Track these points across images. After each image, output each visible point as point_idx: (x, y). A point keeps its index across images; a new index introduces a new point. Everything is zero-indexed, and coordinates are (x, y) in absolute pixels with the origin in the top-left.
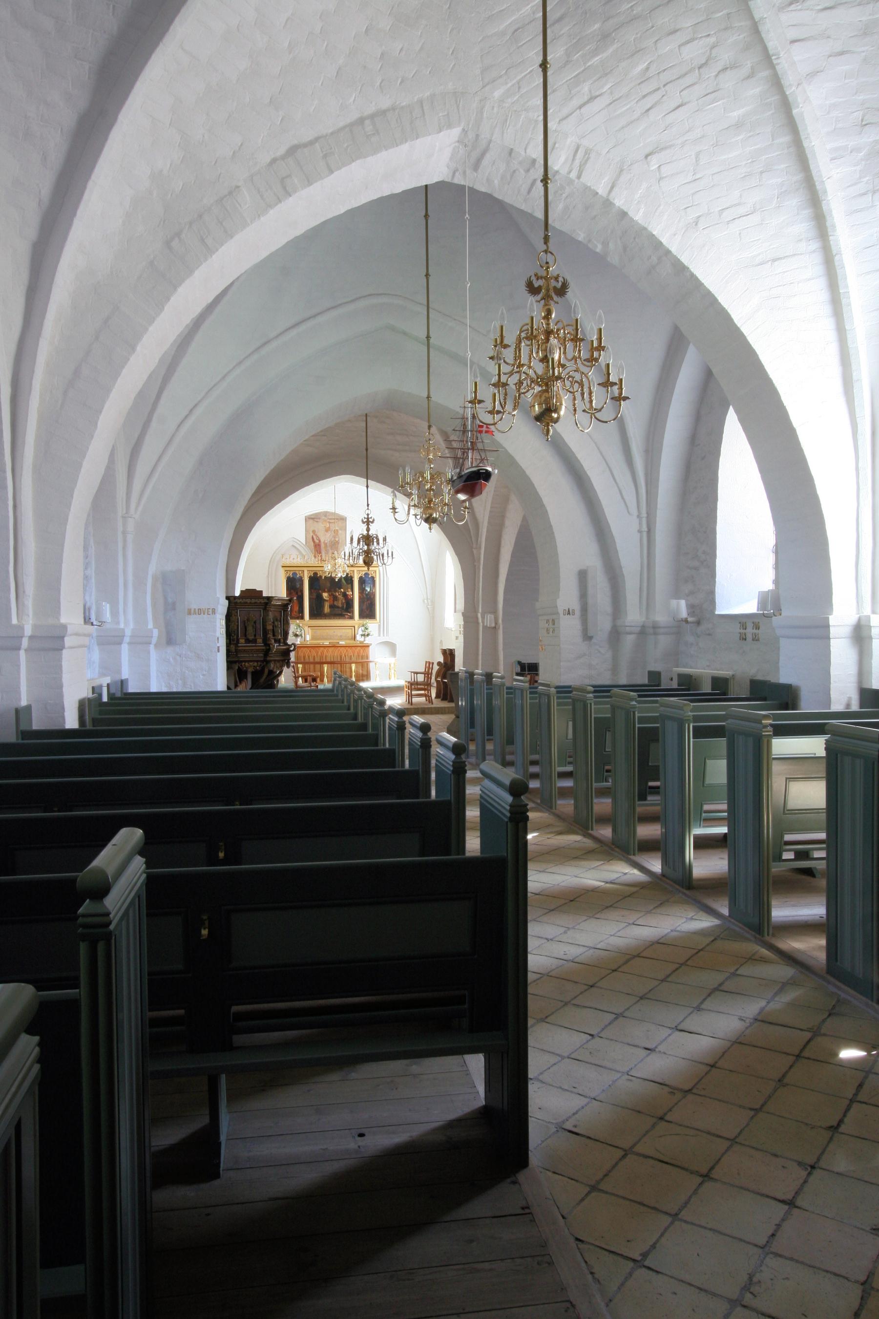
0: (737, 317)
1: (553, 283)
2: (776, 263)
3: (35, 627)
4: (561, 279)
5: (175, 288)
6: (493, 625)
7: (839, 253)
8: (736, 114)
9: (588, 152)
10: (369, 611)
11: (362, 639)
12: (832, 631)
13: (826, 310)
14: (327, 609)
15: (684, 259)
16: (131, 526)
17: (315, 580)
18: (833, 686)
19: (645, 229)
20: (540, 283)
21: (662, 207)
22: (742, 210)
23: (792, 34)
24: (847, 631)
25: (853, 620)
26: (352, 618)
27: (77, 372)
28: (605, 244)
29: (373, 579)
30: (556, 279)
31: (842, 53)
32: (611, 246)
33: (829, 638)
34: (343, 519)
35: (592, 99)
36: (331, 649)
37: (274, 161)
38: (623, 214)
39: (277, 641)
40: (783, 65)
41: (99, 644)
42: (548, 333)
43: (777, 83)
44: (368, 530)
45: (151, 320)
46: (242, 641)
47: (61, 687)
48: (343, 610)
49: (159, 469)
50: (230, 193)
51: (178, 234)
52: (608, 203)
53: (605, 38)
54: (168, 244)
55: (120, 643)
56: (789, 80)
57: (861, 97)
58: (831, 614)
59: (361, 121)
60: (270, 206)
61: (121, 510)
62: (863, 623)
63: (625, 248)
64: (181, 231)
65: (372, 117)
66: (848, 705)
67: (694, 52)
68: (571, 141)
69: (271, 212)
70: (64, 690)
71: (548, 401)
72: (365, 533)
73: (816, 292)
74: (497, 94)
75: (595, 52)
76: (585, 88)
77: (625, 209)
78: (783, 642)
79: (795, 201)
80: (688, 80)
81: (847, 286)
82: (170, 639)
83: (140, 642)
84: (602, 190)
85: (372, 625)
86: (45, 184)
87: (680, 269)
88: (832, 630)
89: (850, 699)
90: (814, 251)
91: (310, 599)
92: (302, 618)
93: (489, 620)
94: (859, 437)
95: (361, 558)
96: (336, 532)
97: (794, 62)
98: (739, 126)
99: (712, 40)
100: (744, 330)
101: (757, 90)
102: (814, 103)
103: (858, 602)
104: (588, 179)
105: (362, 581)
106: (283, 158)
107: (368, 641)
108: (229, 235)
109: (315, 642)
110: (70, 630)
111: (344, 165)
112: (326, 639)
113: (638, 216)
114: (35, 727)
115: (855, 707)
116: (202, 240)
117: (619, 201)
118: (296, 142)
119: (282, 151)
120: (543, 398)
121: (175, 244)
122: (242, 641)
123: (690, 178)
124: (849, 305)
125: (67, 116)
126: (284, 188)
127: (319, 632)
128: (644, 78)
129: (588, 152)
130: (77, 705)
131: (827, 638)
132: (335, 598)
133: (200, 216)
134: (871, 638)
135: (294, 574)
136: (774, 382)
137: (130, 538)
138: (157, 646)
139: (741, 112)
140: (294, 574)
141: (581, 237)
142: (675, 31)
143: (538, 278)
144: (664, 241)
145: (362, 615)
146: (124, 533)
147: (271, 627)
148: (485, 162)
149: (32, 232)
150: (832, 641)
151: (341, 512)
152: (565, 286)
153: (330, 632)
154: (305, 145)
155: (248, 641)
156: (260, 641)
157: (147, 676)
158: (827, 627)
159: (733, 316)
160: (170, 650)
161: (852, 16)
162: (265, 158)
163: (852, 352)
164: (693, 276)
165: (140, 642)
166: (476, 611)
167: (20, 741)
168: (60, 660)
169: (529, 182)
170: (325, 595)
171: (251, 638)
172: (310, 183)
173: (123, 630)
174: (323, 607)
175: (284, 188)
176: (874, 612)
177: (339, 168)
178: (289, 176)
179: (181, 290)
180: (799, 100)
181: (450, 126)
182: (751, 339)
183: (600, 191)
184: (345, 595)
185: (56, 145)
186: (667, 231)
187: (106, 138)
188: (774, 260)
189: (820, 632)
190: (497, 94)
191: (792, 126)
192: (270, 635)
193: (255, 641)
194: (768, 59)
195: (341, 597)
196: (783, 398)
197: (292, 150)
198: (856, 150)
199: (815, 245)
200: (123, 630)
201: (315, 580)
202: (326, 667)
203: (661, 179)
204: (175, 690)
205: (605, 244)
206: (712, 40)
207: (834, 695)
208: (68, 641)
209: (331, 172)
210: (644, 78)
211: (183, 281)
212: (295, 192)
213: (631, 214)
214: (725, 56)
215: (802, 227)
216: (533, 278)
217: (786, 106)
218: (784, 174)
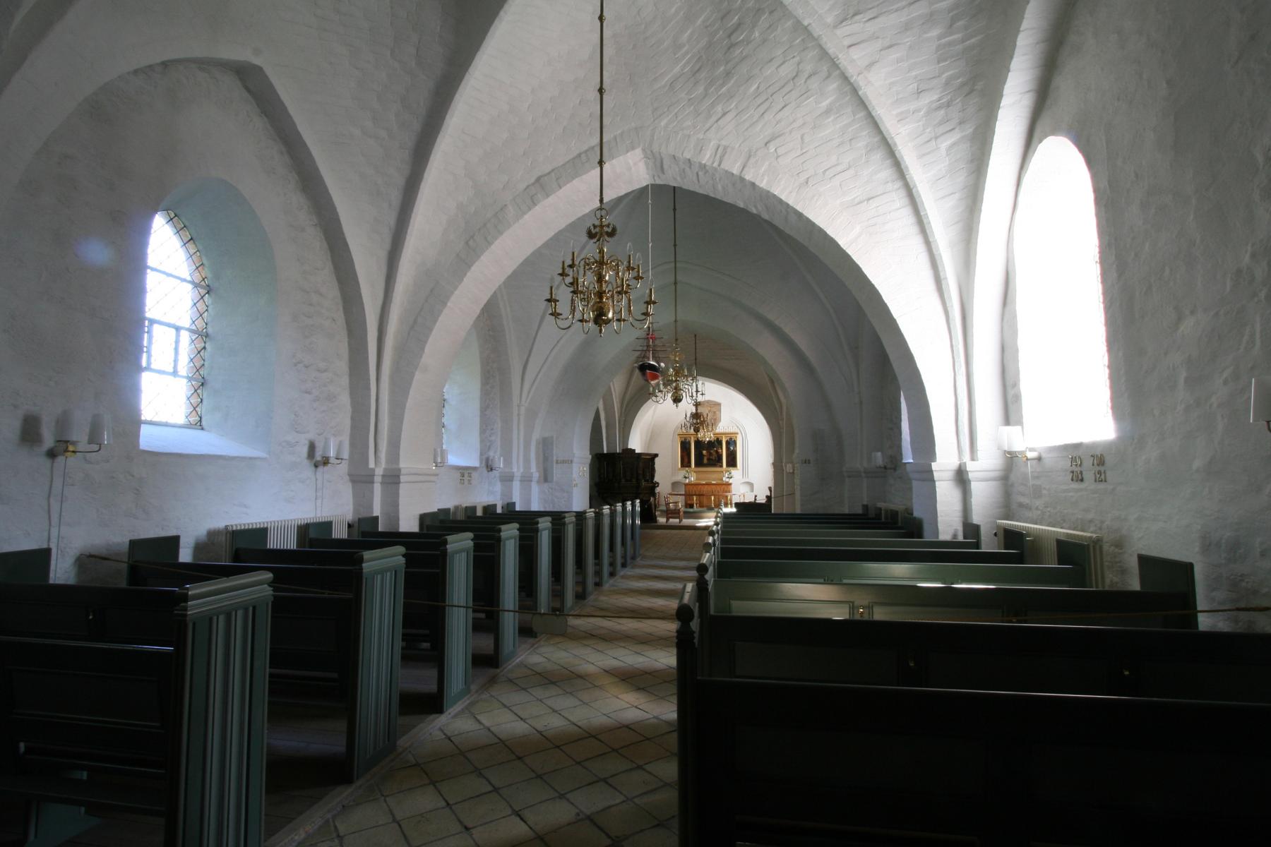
0: (842, 243)
1: (606, 229)
3: (385, 469)
5: (470, 267)
8: (825, 104)
9: (725, 148)
10: (732, 462)
13: (914, 230)
14: (705, 461)
16: (523, 410)
18: (940, 519)
20: (597, 230)
22: (839, 168)
23: (847, 42)
24: (950, 475)
27: (415, 322)
30: (608, 226)
31: (891, 46)
34: (719, 405)
35: (724, 114)
38: (753, 184)
40: (843, 61)
42: (601, 263)
43: (845, 78)
45: (456, 288)
48: (716, 461)
51: (472, 237)
52: (742, 179)
53: (728, 74)
54: (467, 243)
55: (512, 480)
56: (851, 71)
57: (914, 73)
58: (934, 460)
59: (579, 155)
60: (524, 213)
64: (474, 236)
65: (586, 152)
66: (955, 536)
67: (787, 70)
68: (713, 144)
71: (602, 308)
74: (663, 124)
75: (723, 85)
76: (719, 109)
78: (915, 483)
79: (878, 156)
80: (786, 89)
82: (546, 477)
84: (735, 171)
85: (733, 471)
88: (935, 474)
89: (956, 531)
92: (689, 466)
97: (853, 61)
98: (828, 112)
99: (797, 59)
101: (835, 85)
102: (878, 86)
104: (726, 165)
105: (728, 443)
110: (403, 472)
113: (763, 184)
115: (960, 538)
117: (748, 177)
119: (533, 180)
121: (471, 243)
123: (799, 153)
125: (400, 180)
128: (757, 94)
129: (725, 148)
131: (932, 480)
133: (485, 225)
138: (538, 482)
139: (828, 102)
142: (771, 60)
143: (595, 226)
148: (665, 167)
149: (387, 245)
150: (937, 484)
152: (614, 230)
157: (529, 501)
158: (931, 472)
160: (546, 485)
161: (891, 20)
162: (522, 186)
168: (398, 489)
173: (373, 470)
176: (973, 459)
180: (861, 83)
181: (633, 148)
185: (395, 196)
186: (786, 191)
190: (663, 124)
191: (862, 104)
194: (834, 64)
198: (918, 110)
199: (899, 184)
200: (373, 470)
201: (698, 443)
203: (778, 157)
206: (797, 59)
208: (402, 478)
210: (757, 94)
214: (808, 68)
215: (887, 173)
217: (855, 91)
218: (865, 138)
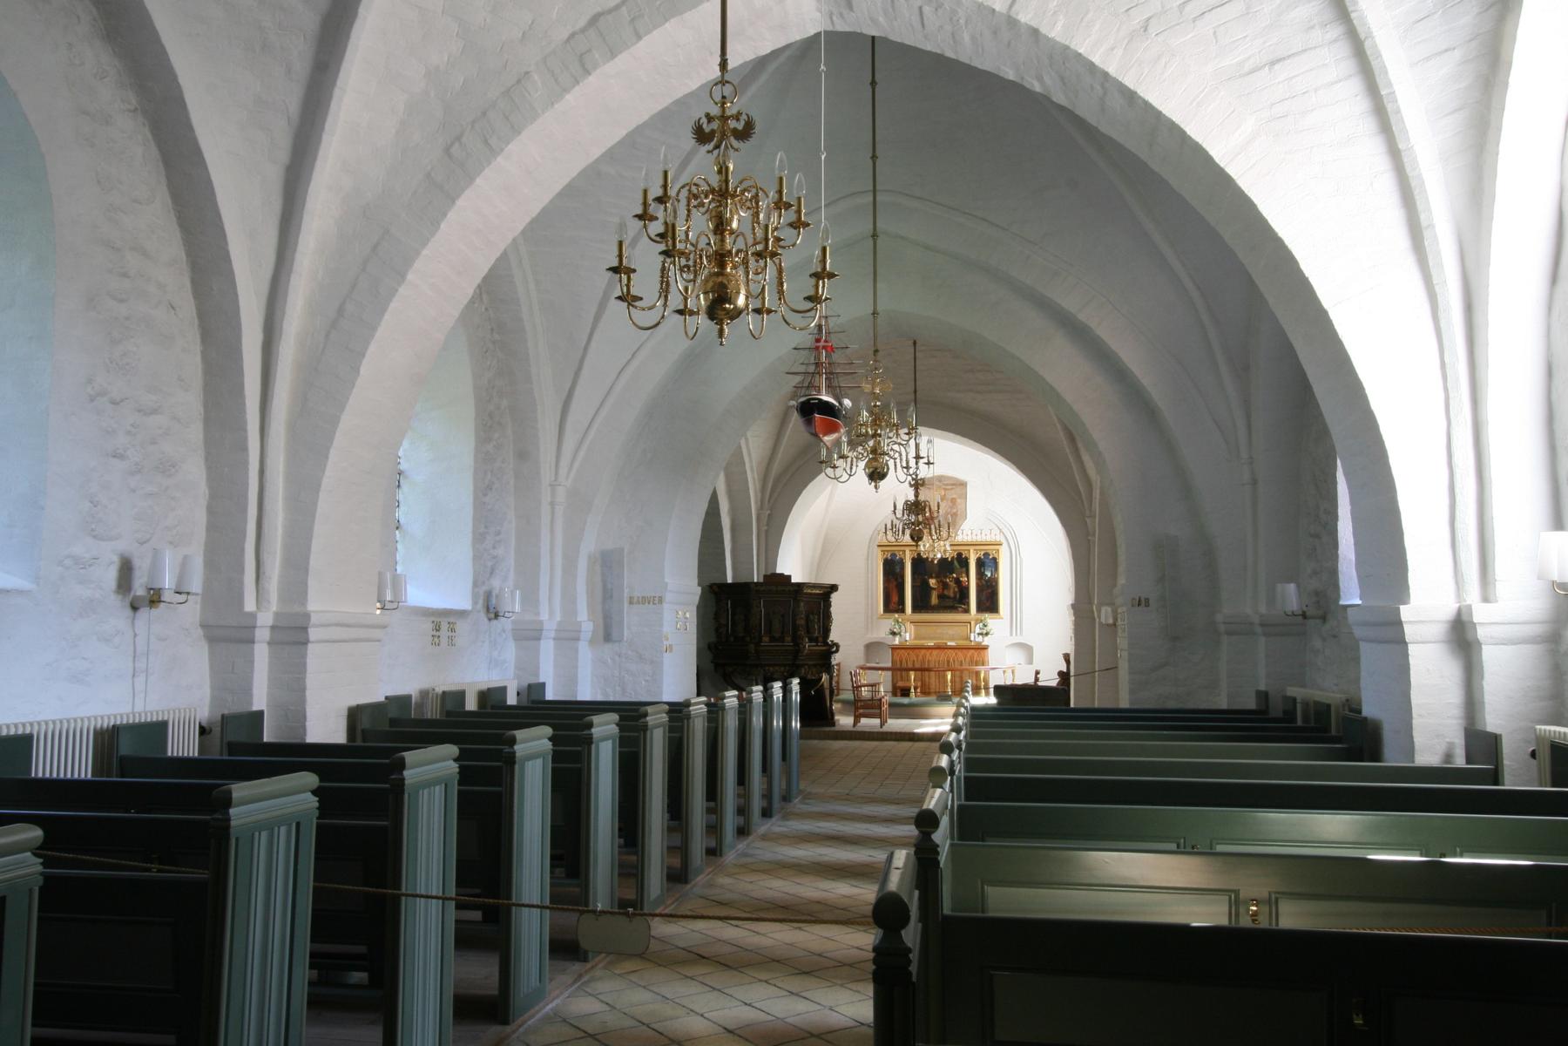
1: (732, 124)
2: (1277, 67)
4: (744, 117)
6: (1111, 621)
7: (1370, 35)
10: (989, 602)
11: (979, 639)
12: (1409, 631)
13: (1366, 126)
14: (934, 600)
15: (1129, 82)
17: (919, 563)
18: (1417, 722)
19: (1067, 48)
20: (715, 125)
21: (1090, 15)
24: (1438, 630)
25: (1446, 608)
26: (967, 611)
27: (341, 311)
28: (1040, 79)
29: (995, 561)
30: (737, 117)
32: (1047, 79)
33: (1406, 644)
36: (935, 652)
37: (573, 35)
38: (1035, 32)
39: (816, 640)
41: (516, 639)
44: (917, 495)
45: (424, 243)
46: (766, 639)
47: (303, 690)
48: (957, 601)
49: (596, 426)
50: (519, 81)
51: (458, 138)
52: (1012, 22)
54: (447, 150)
55: (578, 639)
60: (566, 90)
61: (547, 475)
62: (1465, 618)
63: (1062, 79)
64: (462, 135)
66: (1448, 757)
69: (568, 97)
70: (308, 693)
71: (723, 286)
72: (912, 498)
73: (1349, 100)
77: (1034, 24)
81: (1390, 85)
82: (608, 633)
83: (568, 637)
86: (292, 100)
87: (1130, 96)
88: (1408, 629)
89: (1451, 746)
90: (1335, 41)
91: (913, 587)
92: (903, 611)
93: (1105, 616)
94: (1442, 315)
95: (908, 532)
96: (953, 501)
100: (1230, 171)
103: (1457, 583)
105: (980, 564)
106: (583, 30)
107: (986, 641)
108: (516, 131)
109: (918, 642)
110: (314, 619)
111: (655, 27)
112: (931, 639)
113: (1055, 31)
114: (267, 738)
116: (486, 142)
118: (599, 9)
119: (582, 23)
120: (710, 284)
121: (455, 150)
122: (766, 639)
124: (1398, 111)
126: (583, 66)
127: (924, 630)
130: (345, 713)
131: (1401, 642)
132: (945, 586)
133: (484, 114)
134: (1479, 644)
135: (894, 555)
136: (1287, 242)
137: (559, 510)
140: (894, 555)
141: (1011, 75)
143: (710, 118)
144: (1096, 59)
145: (980, 609)
146: (552, 504)
147: (803, 622)
149: (283, 155)
151: (961, 476)
152: (749, 125)
153: (940, 630)
154: (610, 11)
155: (773, 639)
156: (789, 639)
157: (573, 680)
159: (1212, 153)
160: (608, 647)
163: (1413, 183)
164: (1147, 106)
165: (568, 637)
166: (1091, 603)
167: (225, 757)
168: (304, 656)
169: (917, 12)
170: (932, 582)
171: (777, 635)
172: (613, 54)
173: (253, 616)
174: (929, 597)
175: (583, 66)
176: (1486, 599)
177: (648, 32)
178: (589, 51)
179: (460, 202)
182: (1243, 183)
183: (997, 7)
184: (958, 581)
185: (300, 52)
187: (348, 37)
188: (1273, 63)
189: (1392, 634)
192: (802, 632)
193: (782, 639)
195: (952, 584)
196: (1303, 267)
197: (594, 20)
199: (1336, 31)
200: (253, 616)
201: (919, 563)
202: (912, 675)
204: (611, 699)
205: (1040, 79)
207: (1419, 738)
208: (313, 634)
209: (639, 38)
211: (463, 190)
212: (595, 68)
213: (1043, 30)
216: (704, 120)
